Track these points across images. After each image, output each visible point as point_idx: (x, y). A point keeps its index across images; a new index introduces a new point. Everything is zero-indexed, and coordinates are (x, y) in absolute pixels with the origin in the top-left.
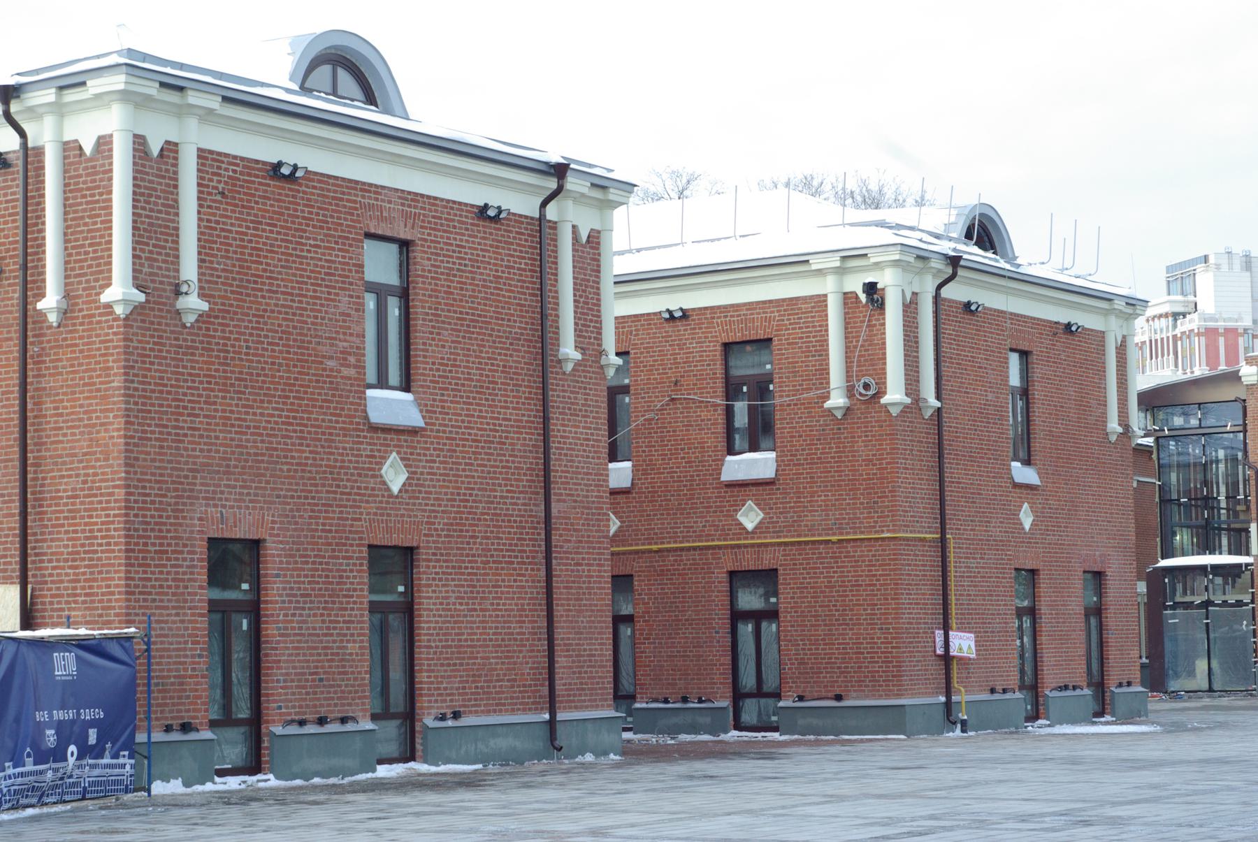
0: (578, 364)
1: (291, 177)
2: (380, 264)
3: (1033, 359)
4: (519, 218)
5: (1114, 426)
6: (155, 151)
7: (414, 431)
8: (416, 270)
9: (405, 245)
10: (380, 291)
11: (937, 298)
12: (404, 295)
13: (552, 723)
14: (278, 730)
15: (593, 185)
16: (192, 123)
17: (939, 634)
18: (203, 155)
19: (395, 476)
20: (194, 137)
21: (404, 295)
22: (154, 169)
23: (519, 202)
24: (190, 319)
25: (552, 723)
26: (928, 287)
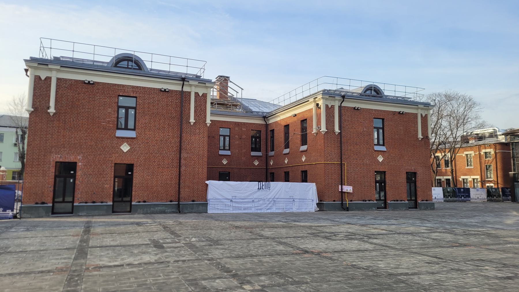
0: (194, 123)
1: (402, 113)
2: (378, 123)
3: (385, 120)
4: (176, 91)
5: (420, 136)
6: (330, 107)
7: (134, 138)
8: (385, 124)
9: (383, 119)
10: (378, 129)
11: (340, 107)
12: (383, 129)
13: (179, 204)
14: (389, 202)
15: (39, 64)
16: (193, 87)
17: (340, 186)
18: (59, 80)
19: (380, 159)
20: (55, 75)
21: (383, 129)
22: (329, 110)
23: (176, 87)
24: (51, 114)
25: (179, 204)
26: (337, 104)
